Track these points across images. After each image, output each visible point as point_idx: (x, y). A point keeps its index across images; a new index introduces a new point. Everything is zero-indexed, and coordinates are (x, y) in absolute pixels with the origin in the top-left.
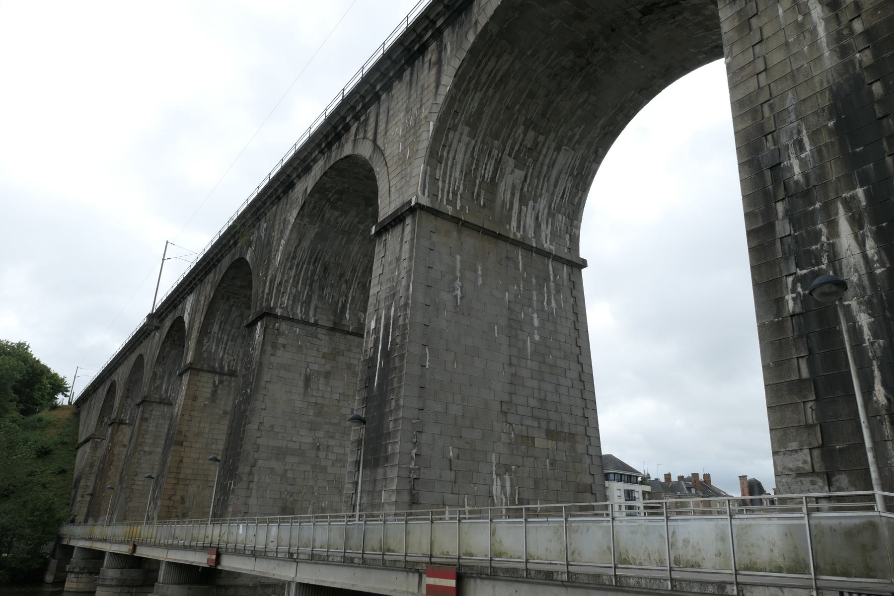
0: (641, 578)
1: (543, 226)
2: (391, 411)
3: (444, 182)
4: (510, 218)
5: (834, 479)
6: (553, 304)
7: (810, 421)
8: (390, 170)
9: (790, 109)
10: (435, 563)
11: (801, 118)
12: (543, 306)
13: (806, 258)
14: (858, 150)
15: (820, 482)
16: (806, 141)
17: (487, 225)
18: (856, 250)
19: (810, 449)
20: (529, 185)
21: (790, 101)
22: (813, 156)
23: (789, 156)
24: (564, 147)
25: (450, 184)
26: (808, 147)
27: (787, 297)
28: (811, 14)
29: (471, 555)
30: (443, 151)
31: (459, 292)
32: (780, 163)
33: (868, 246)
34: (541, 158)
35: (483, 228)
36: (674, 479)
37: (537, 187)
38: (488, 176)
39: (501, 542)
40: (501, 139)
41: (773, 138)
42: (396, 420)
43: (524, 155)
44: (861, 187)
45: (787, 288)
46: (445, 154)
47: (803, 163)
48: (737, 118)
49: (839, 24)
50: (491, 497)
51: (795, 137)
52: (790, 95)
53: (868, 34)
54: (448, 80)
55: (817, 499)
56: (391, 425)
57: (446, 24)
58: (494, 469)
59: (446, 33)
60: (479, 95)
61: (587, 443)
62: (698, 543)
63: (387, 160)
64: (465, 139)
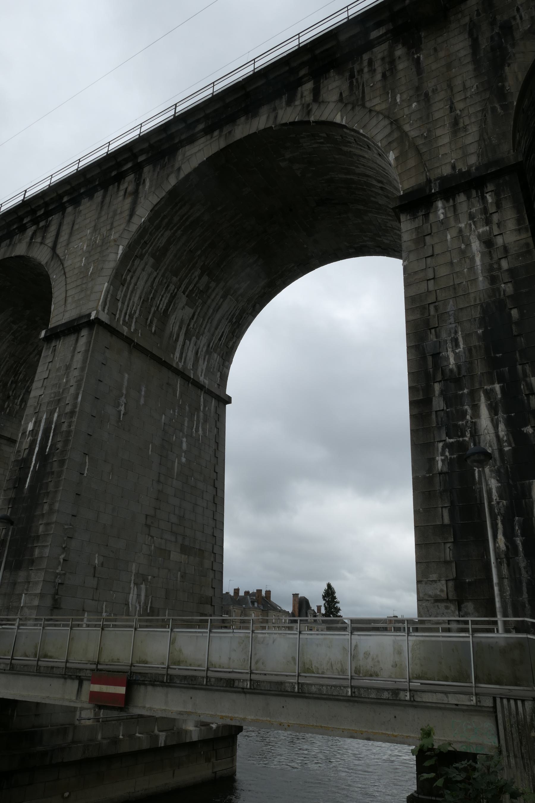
0: (323, 685)
1: (201, 361)
2: (43, 515)
3: (123, 303)
4: (175, 349)
5: (463, 606)
6: (200, 432)
7: (448, 559)
8: (69, 281)
9: (451, 313)
10: (101, 670)
11: (458, 322)
12: (192, 432)
13: (454, 430)
14: (498, 355)
15: (452, 607)
16: (460, 340)
17: (155, 352)
18: (492, 431)
19: (446, 581)
20: (195, 322)
21: (451, 307)
22: (465, 353)
23: (447, 349)
24: (229, 296)
25: (128, 306)
26: (462, 346)
27: (437, 458)
28: (471, 246)
29: (146, 663)
30: (127, 275)
31: (122, 408)
32: (440, 353)
33: (500, 428)
34: (209, 301)
35: (151, 353)
36: (242, 593)
37: (201, 326)
38: (162, 307)
39: (180, 651)
40: (179, 277)
41: (435, 331)
42: (47, 524)
43: (196, 295)
44: (498, 383)
45: (438, 451)
46: (128, 278)
47: (457, 356)
48: (408, 311)
49: (491, 258)
50: (127, 604)
51: (453, 335)
52: (451, 302)
53: (511, 271)
54: (143, 213)
55: (449, 622)
56: (41, 529)
57: (147, 161)
58: (133, 578)
59: (146, 169)
60: (168, 234)
61: (212, 559)
62: (377, 656)
63: (67, 270)
64: (149, 269)
